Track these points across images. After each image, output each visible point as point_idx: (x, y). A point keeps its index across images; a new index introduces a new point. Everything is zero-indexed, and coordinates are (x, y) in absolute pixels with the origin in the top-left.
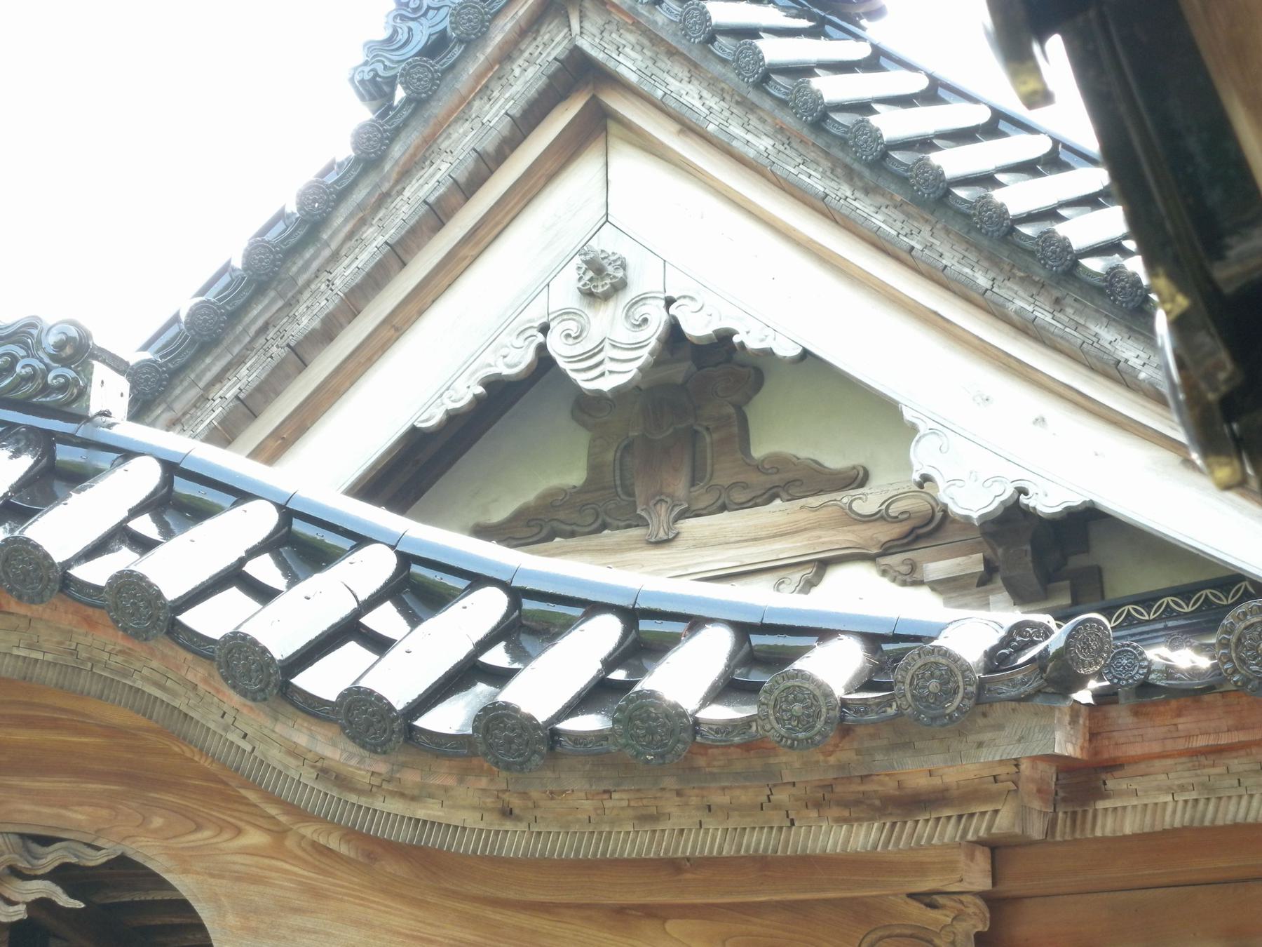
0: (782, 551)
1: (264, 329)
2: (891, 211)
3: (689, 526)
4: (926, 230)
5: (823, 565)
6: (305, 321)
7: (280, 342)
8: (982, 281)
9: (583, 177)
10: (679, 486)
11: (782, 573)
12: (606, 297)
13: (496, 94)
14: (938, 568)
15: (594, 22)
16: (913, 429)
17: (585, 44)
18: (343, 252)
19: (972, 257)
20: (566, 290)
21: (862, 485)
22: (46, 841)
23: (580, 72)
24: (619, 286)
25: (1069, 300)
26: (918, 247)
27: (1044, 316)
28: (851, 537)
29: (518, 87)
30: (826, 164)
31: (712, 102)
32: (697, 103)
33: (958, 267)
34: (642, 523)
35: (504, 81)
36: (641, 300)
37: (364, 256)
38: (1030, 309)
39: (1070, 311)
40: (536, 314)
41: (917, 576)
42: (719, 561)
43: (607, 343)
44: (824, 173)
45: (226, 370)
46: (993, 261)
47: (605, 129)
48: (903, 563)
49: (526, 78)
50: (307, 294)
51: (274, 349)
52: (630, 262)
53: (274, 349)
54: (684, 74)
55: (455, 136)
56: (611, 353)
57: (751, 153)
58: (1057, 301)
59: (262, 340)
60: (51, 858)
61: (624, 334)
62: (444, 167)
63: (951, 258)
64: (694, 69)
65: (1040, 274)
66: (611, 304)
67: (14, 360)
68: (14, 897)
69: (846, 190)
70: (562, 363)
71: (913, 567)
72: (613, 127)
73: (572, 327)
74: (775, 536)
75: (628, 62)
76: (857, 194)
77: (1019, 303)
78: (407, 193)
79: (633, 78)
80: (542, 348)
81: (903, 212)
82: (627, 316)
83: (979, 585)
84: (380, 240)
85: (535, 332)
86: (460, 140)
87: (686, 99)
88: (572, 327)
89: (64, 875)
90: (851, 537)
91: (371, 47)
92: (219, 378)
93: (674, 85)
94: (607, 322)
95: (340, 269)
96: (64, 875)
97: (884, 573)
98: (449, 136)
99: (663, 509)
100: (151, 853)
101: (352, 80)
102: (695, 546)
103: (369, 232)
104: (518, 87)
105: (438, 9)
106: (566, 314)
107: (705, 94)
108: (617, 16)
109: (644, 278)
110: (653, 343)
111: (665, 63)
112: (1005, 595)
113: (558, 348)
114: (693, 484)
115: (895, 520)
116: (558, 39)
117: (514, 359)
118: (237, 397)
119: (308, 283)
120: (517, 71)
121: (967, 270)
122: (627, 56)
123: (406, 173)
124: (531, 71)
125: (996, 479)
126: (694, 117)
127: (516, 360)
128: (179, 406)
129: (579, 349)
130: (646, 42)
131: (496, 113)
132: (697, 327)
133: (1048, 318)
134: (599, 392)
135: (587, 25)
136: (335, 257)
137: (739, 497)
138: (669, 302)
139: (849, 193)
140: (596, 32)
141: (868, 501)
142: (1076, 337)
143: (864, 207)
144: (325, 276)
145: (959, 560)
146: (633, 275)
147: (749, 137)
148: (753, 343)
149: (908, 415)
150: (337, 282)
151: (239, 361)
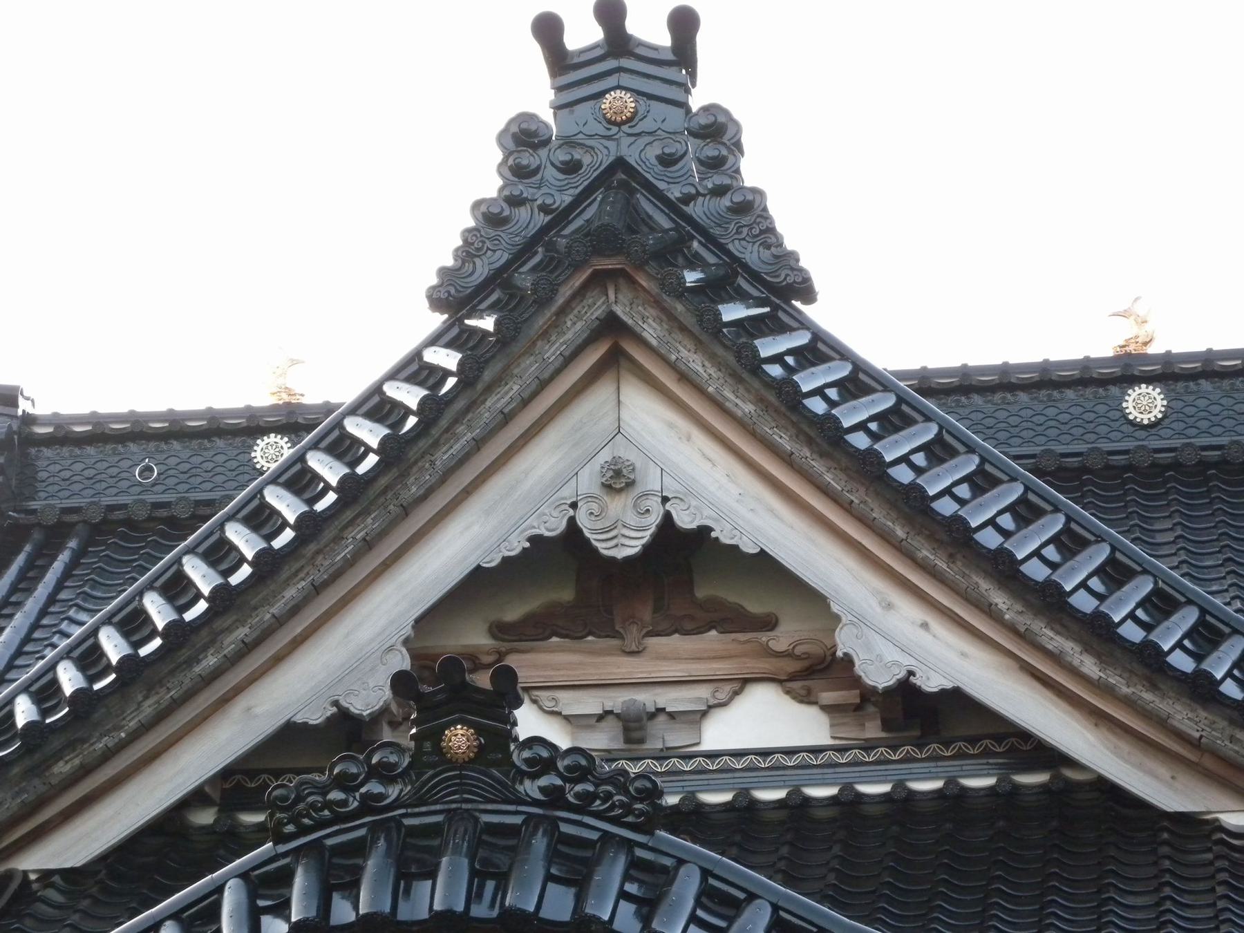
0: (719, 669)
2: (838, 472)
3: (653, 642)
4: (862, 490)
5: (745, 682)
6: (414, 489)
7: (396, 502)
8: (900, 532)
9: (601, 394)
10: (646, 614)
11: (716, 685)
12: (620, 491)
13: (553, 338)
14: (828, 697)
15: (626, 295)
16: (837, 619)
17: (618, 310)
18: (442, 441)
19: (894, 515)
20: (588, 480)
21: (772, 629)
23: (611, 326)
24: (631, 484)
25: (959, 556)
26: (856, 501)
27: (942, 564)
28: (767, 666)
29: (569, 335)
30: (793, 431)
31: (712, 371)
32: (701, 370)
33: (883, 520)
34: (616, 635)
35: (559, 329)
36: (645, 495)
37: (457, 447)
38: (932, 557)
39: (959, 563)
40: (567, 493)
41: (812, 699)
43: (620, 523)
44: (791, 437)
46: (908, 520)
47: (617, 362)
48: (803, 687)
49: (575, 329)
50: (415, 469)
51: (391, 507)
52: (638, 465)
53: (391, 507)
54: (692, 347)
55: (523, 366)
56: (624, 535)
57: (740, 413)
59: (382, 499)
61: (632, 519)
62: (516, 388)
63: (878, 513)
64: (699, 345)
65: (943, 536)
66: (623, 495)
69: (806, 452)
70: (587, 534)
71: (809, 691)
72: (623, 362)
73: (595, 507)
74: (714, 658)
75: (651, 331)
76: (815, 456)
77: (925, 553)
78: (488, 404)
79: (654, 342)
80: (572, 521)
81: (848, 475)
82: (635, 506)
83: (855, 710)
84: (469, 436)
85: (567, 507)
86: (526, 369)
87: (692, 365)
88: (595, 507)
90: (767, 666)
92: (351, 523)
93: (684, 353)
94: (618, 507)
95: (439, 454)
97: (788, 693)
98: (519, 365)
99: (634, 629)
102: (657, 658)
103: (461, 429)
104: (569, 335)
105: (494, 251)
106: (590, 497)
107: (706, 363)
109: (651, 481)
110: (653, 529)
111: (679, 336)
112: (879, 722)
113: (583, 521)
114: (654, 612)
115: (798, 658)
116: (599, 303)
117: (553, 526)
118: (364, 539)
119: (416, 462)
120: (569, 323)
121: (890, 524)
122: (649, 325)
123: (489, 389)
124: (579, 325)
125: (896, 663)
126: (698, 380)
127: (554, 526)
128: (323, 541)
129: (599, 525)
130: (664, 318)
131: (553, 351)
132: (685, 520)
133: (945, 567)
134: (613, 559)
135: (620, 297)
136: (436, 444)
137: (688, 626)
138: (665, 500)
139: (808, 454)
140: (627, 303)
141: (781, 640)
142: (963, 583)
143: (818, 466)
144: (428, 457)
145: (843, 693)
146: (638, 476)
147: (738, 401)
148: (726, 540)
149: (835, 608)
150: (438, 463)
151: (365, 512)
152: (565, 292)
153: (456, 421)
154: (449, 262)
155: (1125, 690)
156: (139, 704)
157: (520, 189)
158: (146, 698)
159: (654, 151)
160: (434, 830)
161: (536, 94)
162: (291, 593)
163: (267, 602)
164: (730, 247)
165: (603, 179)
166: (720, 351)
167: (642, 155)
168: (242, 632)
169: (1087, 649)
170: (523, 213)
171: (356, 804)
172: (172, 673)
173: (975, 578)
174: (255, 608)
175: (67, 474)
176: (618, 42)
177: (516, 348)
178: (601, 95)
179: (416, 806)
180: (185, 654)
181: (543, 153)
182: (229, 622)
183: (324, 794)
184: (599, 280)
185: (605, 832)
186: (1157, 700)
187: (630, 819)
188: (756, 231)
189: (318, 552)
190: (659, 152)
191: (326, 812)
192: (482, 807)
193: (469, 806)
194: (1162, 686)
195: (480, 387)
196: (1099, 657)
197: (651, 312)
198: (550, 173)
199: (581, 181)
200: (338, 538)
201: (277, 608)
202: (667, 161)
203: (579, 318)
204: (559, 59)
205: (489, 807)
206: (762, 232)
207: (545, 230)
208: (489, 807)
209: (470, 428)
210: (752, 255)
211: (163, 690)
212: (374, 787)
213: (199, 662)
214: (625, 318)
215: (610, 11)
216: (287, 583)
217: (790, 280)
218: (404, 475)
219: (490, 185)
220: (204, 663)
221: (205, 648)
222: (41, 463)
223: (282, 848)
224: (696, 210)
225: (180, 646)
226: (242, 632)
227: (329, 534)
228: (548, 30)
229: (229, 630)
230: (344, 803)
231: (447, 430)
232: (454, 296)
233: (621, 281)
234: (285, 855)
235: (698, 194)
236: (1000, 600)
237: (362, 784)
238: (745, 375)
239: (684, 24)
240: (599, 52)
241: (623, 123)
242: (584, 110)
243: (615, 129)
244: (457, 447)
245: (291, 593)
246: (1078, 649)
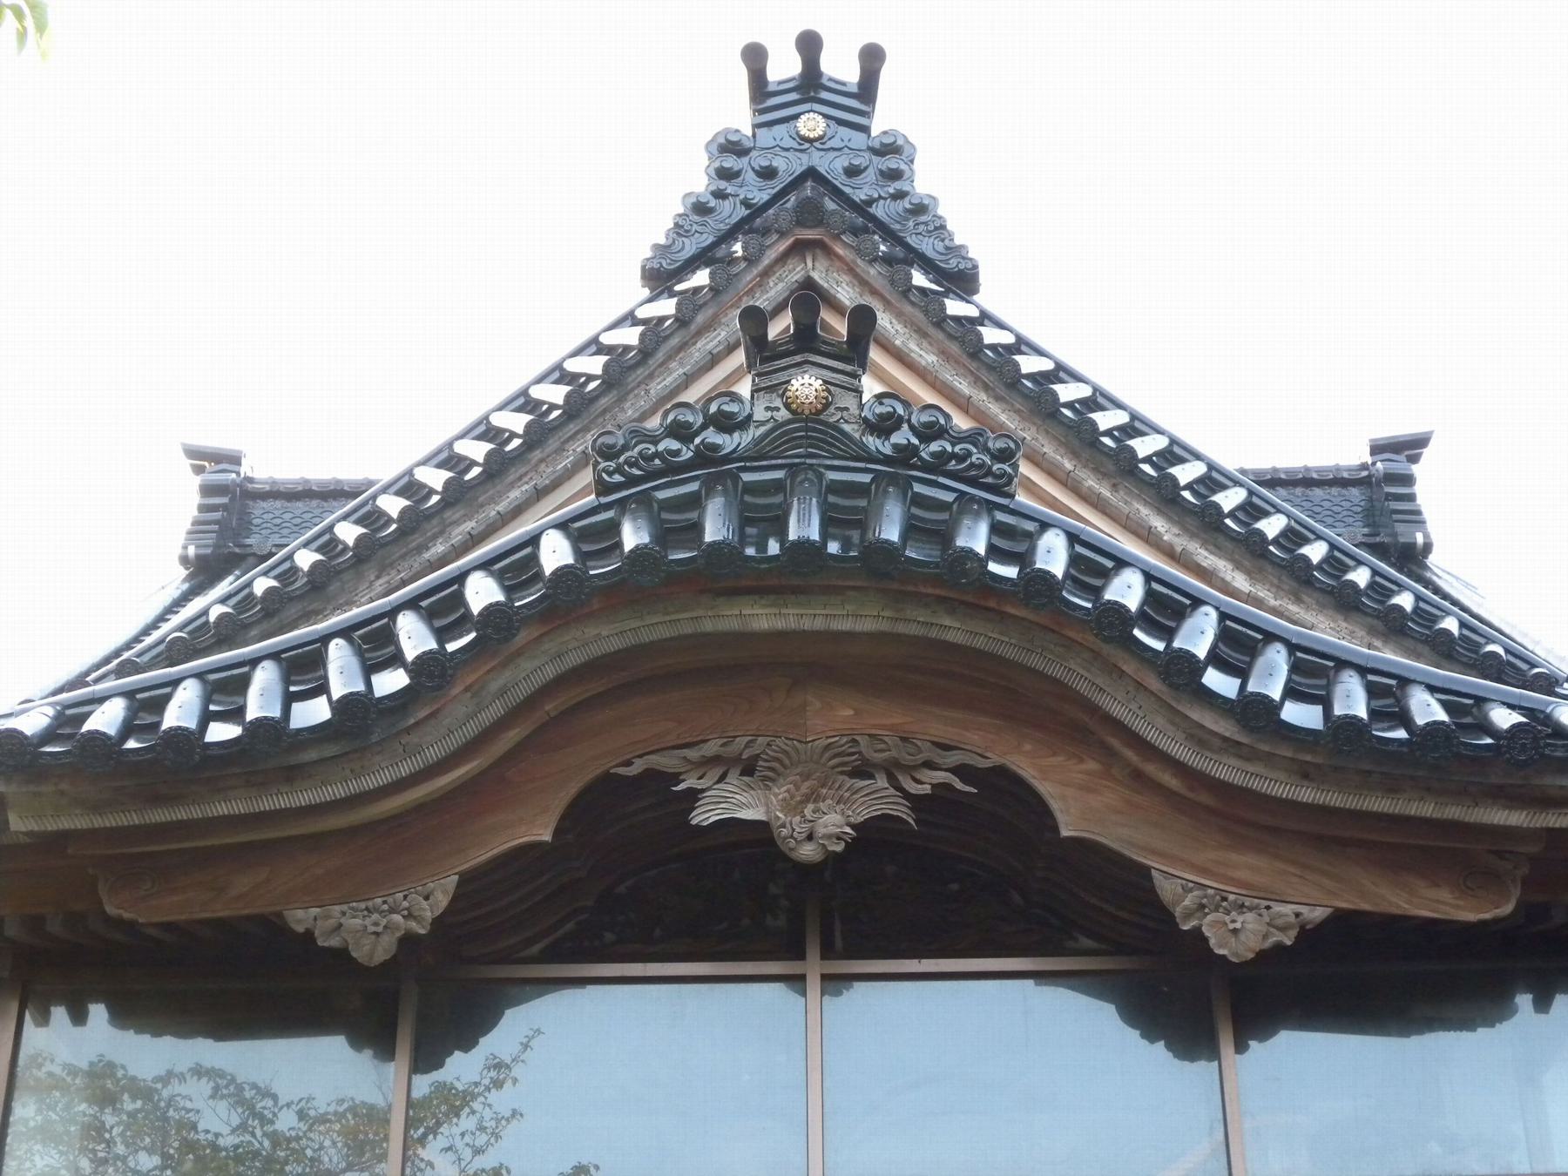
1: (604, 412)
4: (1034, 429)
15: (822, 264)
17: (816, 276)
19: (1062, 451)
22: (947, 748)
27: (1106, 492)
29: (772, 293)
31: (899, 327)
37: (669, 379)
42: (404, 583)
45: (577, 433)
46: (1075, 455)
58: (1114, 485)
60: (954, 759)
65: (1111, 467)
67: (970, 454)
68: (924, 779)
78: (699, 345)
84: (681, 371)
89: (960, 771)
91: (656, 247)
92: (572, 438)
96: (960, 771)
100: (1026, 767)
101: (643, 267)
103: (673, 365)
104: (772, 293)
108: (838, 264)
119: (633, 390)
123: (699, 333)
124: (781, 286)
128: (548, 450)
136: (651, 376)
152: (771, 255)
153: (670, 357)
154: (662, 241)
155: (1273, 602)
156: (371, 583)
157: (723, 184)
158: (378, 577)
159: (841, 163)
160: (777, 486)
161: (740, 118)
162: (515, 495)
163: (493, 501)
164: (908, 240)
165: (796, 183)
166: (908, 309)
167: (832, 166)
168: (469, 525)
169: (1238, 566)
170: (726, 205)
171: (690, 454)
172: (403, 557)
173: (1137, 506)
174: (482, 506)
175: (278, 521)
176: (811, 83)
177: (725, 298)
178: (796, 117)
179: (756, 459)
180: (416, 540)
181: (745, 160)
182: (457, 516)
183: (655, 443)
184: (800, 249)
185: (962, 494)
186: (1302, 612)
187: (989, 480)
188: (931, 228)
189: (542, 460)
190: (846, 164)
191: (657, 461)
192: (828, 462)
193: (814, 461)
194: (1305, 598)
195: (693, 327)
196: (1249, 573)
197: (845, 278)
198: (750, 176)
199: (777, 185)
200: (561, 450)
201: (502, 507)
202: (852, 172)
203: (780, 280)
204: (759, 87)
205: (836, 463)
206: (936, 228)
207: (744, 221)
208: (836, 463)
209: (681, 364)
210: (927, 246)
211: (394, 572)
212: (712, 436)
213: (428, 549)
214: (821, 282)
215: (809, 45)
216: (512, 486)
217: (961, 267)
218: (621, 400)
219: (700, 184)
220: (433, 550)
221: (434, 537)
222: (257, 512)
223: (604, 500)
224: (878, 210)
225: (413, 530)
226: (469, 525)
227: (553, 443)
228: (755, 57)
229: (457, 523)
230: (677, 453)
231: (661, 365)
232: (659, 278)
233: (818, 251)
234: (608, 506)
235: (880, 197)
236: (1159, 524)
237: (697, 433)
238: (931, 330)
239: (872, 58)
240: (791, 85)
241: (816, 140)
242: (780, 130)
243: (807, 145)
244: (669, 379)
245: (515, 495)
246: (1230, 567)
